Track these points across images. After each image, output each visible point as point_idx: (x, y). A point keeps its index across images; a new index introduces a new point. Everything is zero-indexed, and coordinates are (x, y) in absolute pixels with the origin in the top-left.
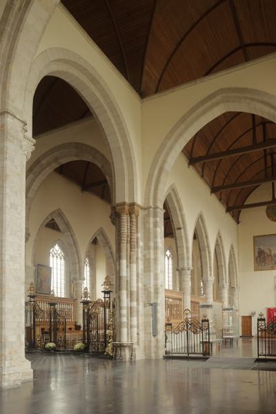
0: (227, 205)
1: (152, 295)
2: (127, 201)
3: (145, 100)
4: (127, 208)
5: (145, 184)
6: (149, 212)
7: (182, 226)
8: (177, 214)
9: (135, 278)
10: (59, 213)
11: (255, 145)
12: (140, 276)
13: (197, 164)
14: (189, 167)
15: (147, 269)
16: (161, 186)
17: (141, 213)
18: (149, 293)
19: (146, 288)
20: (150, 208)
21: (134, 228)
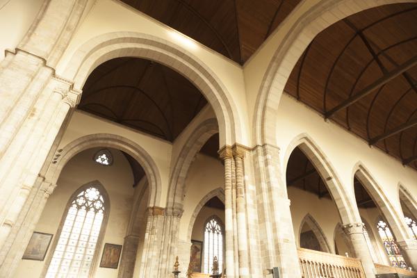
0: (402, 158)
1: (272, 255)
2: (229, 143)
3: (245, 65)
4: (228, 151)
5: (252, 124)
6: (257, 151)
7: (331, 175)
8: (320, 163)
9: (243, 231)
10: (221, 191)
11: (387, 74)
12: (252, 229)
13: (333, 115)
14: (325, 121)
15: (262, 219)
16: (396, 209)
17: (248, 155)
18: (267, 253)
19: (263, 246)
20: (257, 146)
21: (240, 170)
